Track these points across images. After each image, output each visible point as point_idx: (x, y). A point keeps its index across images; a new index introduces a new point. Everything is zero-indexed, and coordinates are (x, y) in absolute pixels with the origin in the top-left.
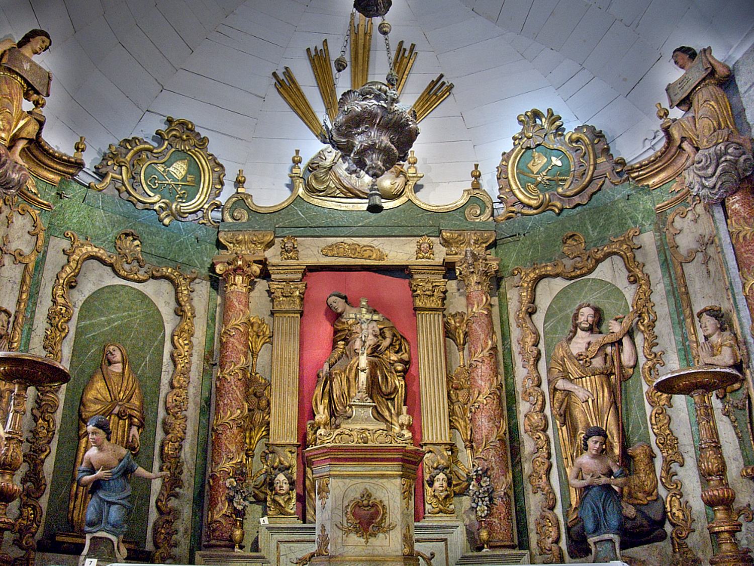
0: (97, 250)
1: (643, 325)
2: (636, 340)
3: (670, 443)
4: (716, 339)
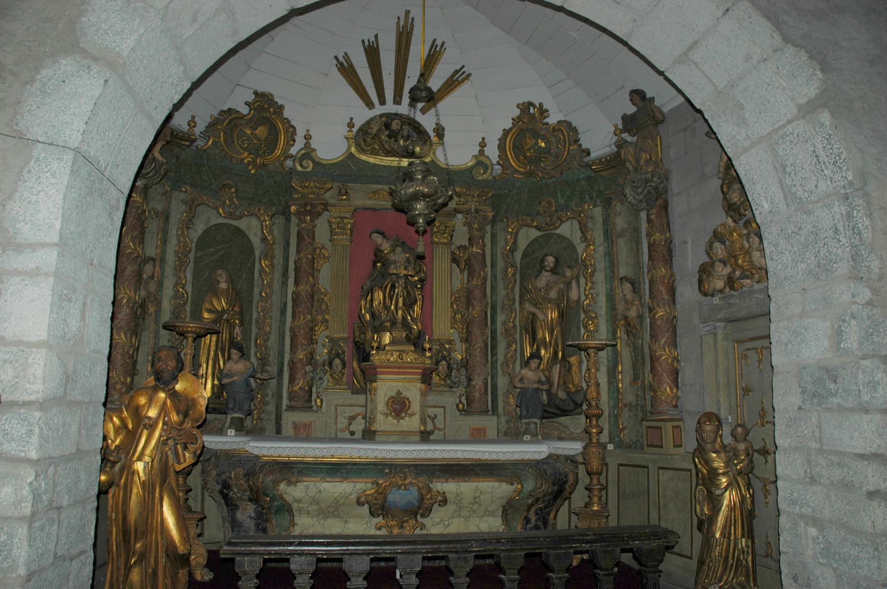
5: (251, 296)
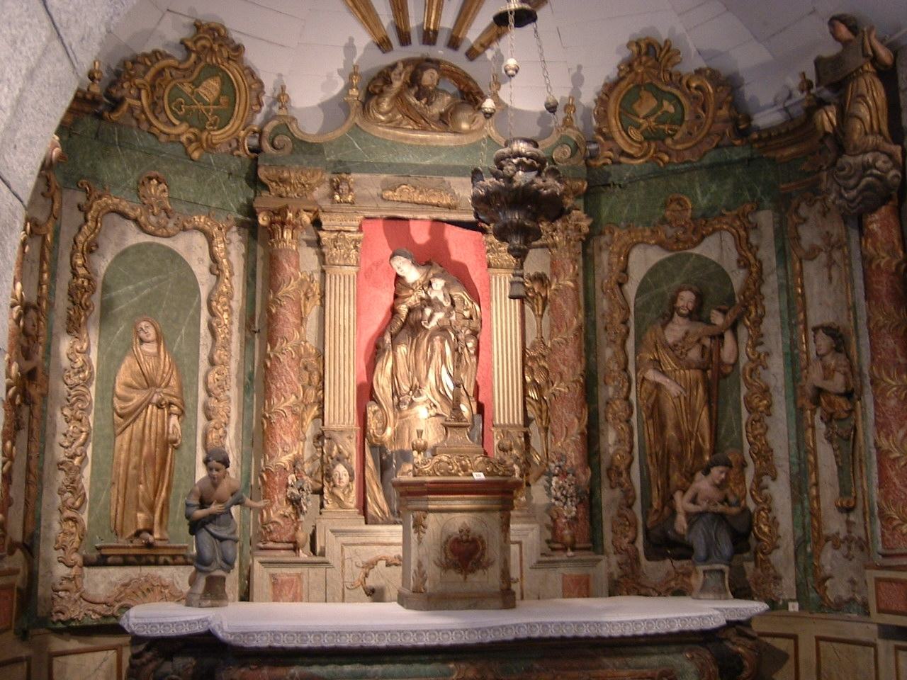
0: (116, 201)
1: (749, 320)
2: (739, 334)
3: (764, 455)
4: (831, 361)
5: (196, 363)
